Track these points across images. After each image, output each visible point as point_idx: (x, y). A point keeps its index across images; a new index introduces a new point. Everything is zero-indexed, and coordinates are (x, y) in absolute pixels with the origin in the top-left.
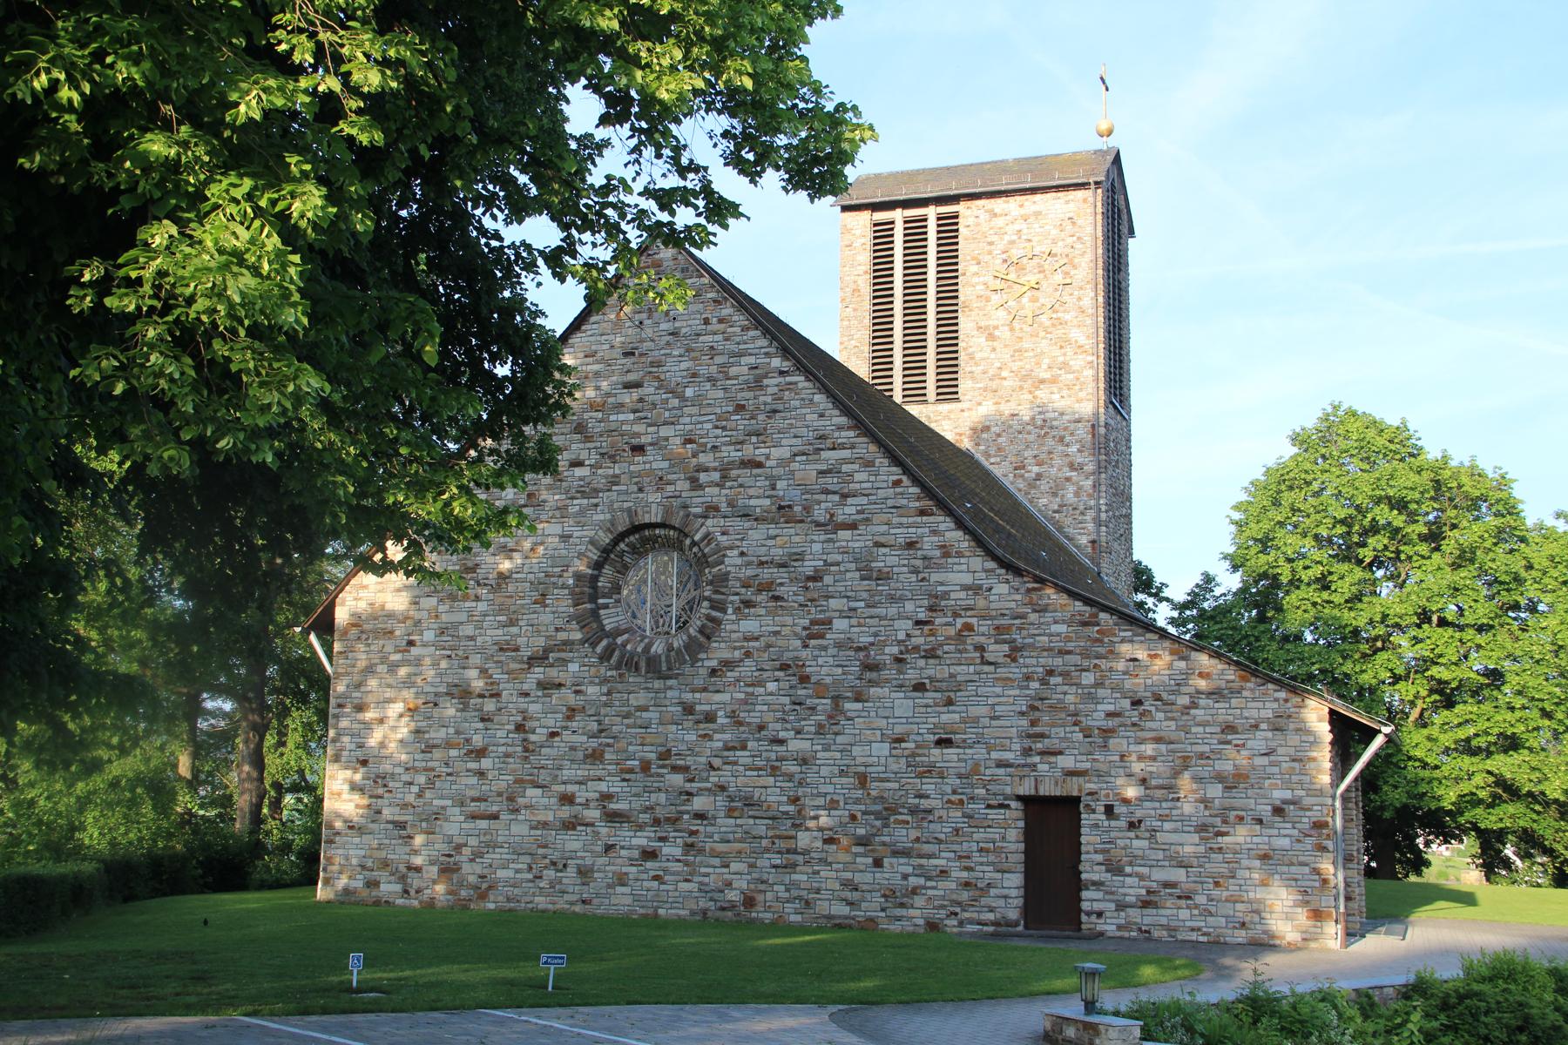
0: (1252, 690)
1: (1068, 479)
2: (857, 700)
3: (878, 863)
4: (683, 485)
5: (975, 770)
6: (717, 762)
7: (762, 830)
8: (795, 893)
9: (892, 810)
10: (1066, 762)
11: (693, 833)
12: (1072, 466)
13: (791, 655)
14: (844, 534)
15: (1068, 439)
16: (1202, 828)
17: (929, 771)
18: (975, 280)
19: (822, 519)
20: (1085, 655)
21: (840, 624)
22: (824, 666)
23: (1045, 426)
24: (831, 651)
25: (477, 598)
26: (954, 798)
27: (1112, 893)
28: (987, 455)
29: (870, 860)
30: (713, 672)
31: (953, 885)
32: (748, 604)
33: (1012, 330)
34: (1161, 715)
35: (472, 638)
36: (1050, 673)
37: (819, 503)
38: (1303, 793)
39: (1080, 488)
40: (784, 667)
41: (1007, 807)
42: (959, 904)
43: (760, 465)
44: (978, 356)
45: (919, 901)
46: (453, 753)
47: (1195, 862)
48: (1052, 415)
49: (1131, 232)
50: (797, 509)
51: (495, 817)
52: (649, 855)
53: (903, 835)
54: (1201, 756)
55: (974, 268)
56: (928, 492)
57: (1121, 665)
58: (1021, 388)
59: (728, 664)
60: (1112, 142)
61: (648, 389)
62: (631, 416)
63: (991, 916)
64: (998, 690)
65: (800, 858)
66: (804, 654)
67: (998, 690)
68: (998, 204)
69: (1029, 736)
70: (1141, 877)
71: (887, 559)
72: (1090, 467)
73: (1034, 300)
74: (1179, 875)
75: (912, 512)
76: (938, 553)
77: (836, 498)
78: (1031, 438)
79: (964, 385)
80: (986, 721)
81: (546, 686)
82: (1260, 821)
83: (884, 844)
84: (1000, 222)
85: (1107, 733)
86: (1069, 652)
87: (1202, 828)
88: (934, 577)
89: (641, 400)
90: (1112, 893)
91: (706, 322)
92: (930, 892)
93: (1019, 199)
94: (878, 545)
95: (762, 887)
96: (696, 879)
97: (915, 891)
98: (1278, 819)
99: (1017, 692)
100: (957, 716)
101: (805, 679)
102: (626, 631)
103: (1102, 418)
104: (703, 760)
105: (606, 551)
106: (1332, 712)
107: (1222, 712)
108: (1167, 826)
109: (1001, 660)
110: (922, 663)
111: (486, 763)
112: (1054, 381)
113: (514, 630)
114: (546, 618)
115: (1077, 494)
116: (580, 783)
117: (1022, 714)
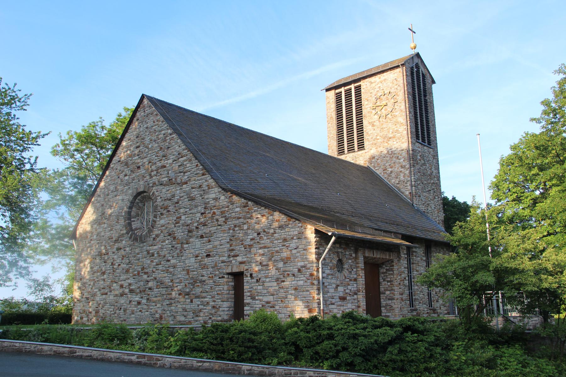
0: (292, 224)
1: (401, 172)
2: (187, 244)
3: (192, 301)
4: (148, 177)
5: (216, 265)
6: (154, 270)
7: (164, 292)
8: (172, 313)
9: (195, 282)
10: (239, 259)
11: (149, 295)
12: (402, 167)
13: (171, 230)
14: (185, 186)
15: (400, 157)
16: (277, 280)
17: (204, 267)
18: (367, 106)
19: (179, 182)
20: (245, 218)
21: (183, 217)
22: (180, 233)
23: (392, 154)
24: (181, 227)
25: (104, 223)
26: (211, 275)
27: (252, 307)
28: (375, 167)
29: (189, 300)
30: (154, 239)
31: (210, 308)
32: (162, 214)
33: (379, 122)
34: (265, 238)
35: (103, 236)
36: (235, 226)
37: (179, 176)
38: (307, 263)
39: (405, 174)
40: (170, 235)
41: (223, 277)
42: (212, 314)
43: (165, 167)
44: (369, 133)
45: (202, 314)
46: (99, 274)
47: (275, 293)
48: (394, 149)
49: (433, 82)
50: (174, 179)
51: (106, 294)
52: (139, 303)
53: (198, 290)
54: (277, 252)
55: (366, 103)
56: (205, 168)
57: (253, 221)
58: (384, 141)
59: (157, 236)
60: (416, 51)
61: (141, 148)
62: (137, 157)
63: (219, 318)
64: (222, 235)
65: (173, 301)
66: (175, 229)
67: (222, 235)
68: (373, 79)
69: (230, 250)
70: (261, 300)
71: (195, 193)
72: (408, 166)
73: (386, 110)
74: (270, 298)
75: (201, 175)
76: (207, 188)
77: (182, 174)
78: (388, 159)
79: (366, 144)
80: (218, 247)
81: (119, 249)
82: (294, 275)
83: (193, 294)
84: (373, 85)
85: (251, 246)
86: (240, 218)
87: (277, 280)
88: (206, 197)
89: (139, 151)
90: (252, 307)
91: (154, 122)
92: (205, 311)
93: (379, 76)
94: (193, 188)
95: (164, 312)
96: (149, 310)
97: (200, 311)
98: (300, 274)
99: (226, 235)
100: (211, 246)
101: (174, 238)
102: (139, 229)
103: (410, 148)
104: (151, 269)
105: (132, 203)
106: (316, 230)
107: (283, 234)
108: (268, 280)
109: (222, 224)
110: (203, 227)
111: (105, 276)
112: (394, 137)
113: (112, 232)
114: (118, 227)
115: (404, 176)
116: (125, 280)
117: (228, 242)
